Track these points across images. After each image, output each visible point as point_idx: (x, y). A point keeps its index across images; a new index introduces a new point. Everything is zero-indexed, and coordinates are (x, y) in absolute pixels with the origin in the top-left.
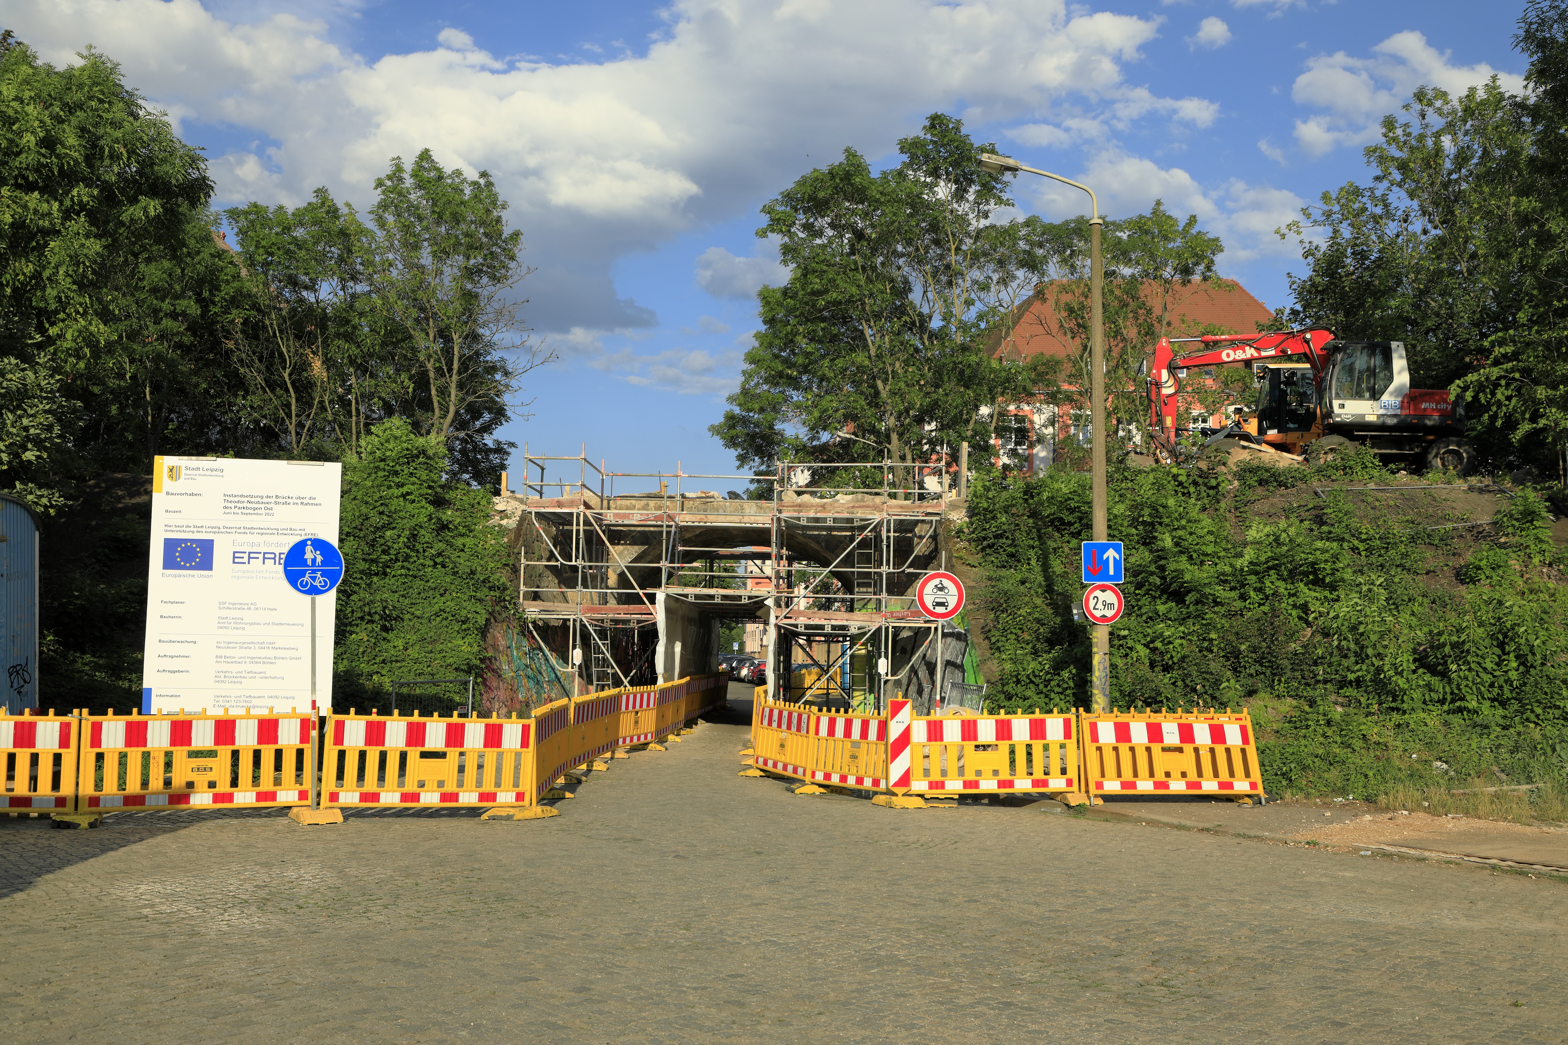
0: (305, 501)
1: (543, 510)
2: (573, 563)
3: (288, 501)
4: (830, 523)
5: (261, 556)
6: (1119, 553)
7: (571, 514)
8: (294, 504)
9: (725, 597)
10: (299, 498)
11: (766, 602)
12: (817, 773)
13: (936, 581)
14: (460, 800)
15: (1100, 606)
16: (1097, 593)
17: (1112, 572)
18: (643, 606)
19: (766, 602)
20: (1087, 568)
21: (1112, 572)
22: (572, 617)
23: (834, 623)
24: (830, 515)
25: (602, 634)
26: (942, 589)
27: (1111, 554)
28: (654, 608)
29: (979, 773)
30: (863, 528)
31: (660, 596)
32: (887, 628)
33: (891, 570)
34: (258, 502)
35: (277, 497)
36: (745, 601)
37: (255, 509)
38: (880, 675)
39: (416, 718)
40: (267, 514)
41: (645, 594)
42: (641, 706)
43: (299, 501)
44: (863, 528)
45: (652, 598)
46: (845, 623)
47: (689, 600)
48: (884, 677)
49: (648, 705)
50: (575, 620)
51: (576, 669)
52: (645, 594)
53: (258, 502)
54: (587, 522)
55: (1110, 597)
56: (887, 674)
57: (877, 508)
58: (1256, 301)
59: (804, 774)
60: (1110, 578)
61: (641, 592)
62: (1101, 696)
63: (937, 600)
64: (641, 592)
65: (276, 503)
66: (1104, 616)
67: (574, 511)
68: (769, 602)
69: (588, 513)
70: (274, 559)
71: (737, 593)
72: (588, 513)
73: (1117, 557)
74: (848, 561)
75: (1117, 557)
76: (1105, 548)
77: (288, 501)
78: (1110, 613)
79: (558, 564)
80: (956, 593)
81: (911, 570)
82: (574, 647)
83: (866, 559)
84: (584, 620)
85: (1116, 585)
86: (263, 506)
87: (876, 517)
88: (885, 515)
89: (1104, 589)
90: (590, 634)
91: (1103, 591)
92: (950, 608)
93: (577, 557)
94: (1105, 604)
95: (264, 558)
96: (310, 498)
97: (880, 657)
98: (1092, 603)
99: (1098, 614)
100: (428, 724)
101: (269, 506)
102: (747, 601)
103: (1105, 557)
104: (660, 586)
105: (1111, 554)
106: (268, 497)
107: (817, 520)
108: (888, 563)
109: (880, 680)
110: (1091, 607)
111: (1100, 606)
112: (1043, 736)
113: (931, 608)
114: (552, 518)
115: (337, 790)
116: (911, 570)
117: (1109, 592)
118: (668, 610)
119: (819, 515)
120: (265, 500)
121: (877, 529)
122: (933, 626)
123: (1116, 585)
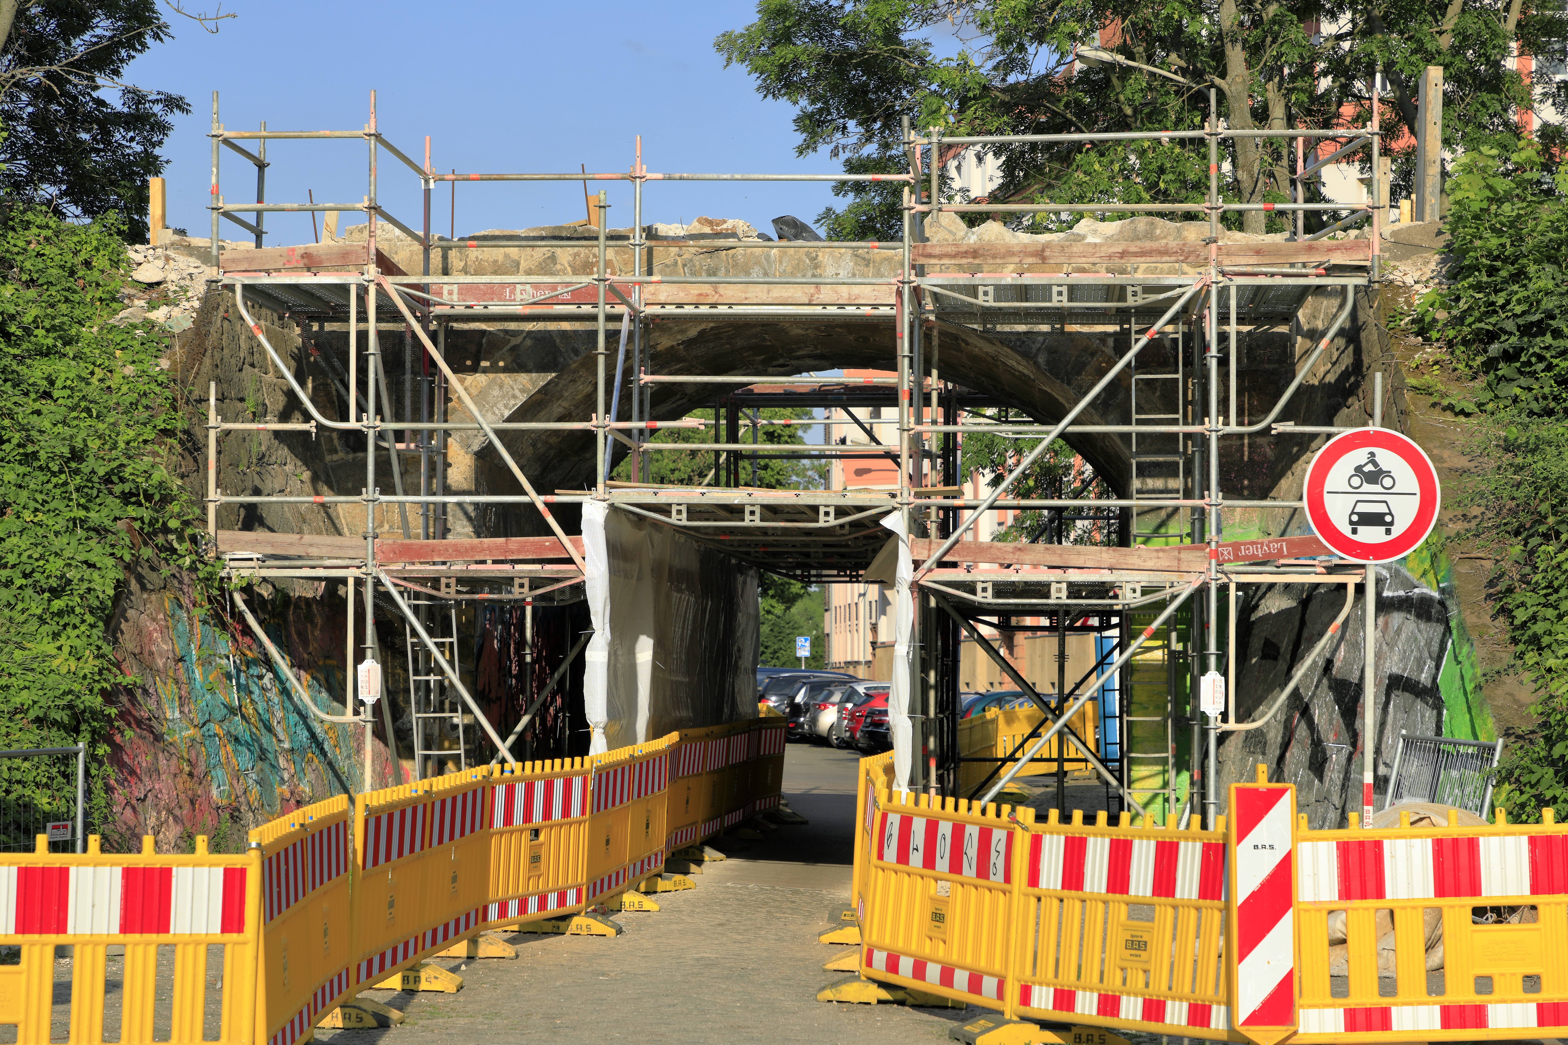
2: (352, 424)
4: (1059, 301)
7: (343, 289)
13: (1359, 456)
18: (547, 541)
22: (351, 574)
23: (1075, 576)
26: (1375, 476)
28: (578, 546)
29: (1484, 984)
32: (1223, 590)
33: (1233, 428)
47: (674, 519)
50: (359, 583)
63: (1362, 508)
67: (352, 279)
69: (390, 283)
71: (806, 498)
79: (311, 427)
80: (1415, 487)
82: (360, 657)
88: (1213, 275)
92: (1398, 530)
93: (361, 409)
102: (832, 521)
107: (1023, 292)
108: (1224, 409)
113: (1345, 529)
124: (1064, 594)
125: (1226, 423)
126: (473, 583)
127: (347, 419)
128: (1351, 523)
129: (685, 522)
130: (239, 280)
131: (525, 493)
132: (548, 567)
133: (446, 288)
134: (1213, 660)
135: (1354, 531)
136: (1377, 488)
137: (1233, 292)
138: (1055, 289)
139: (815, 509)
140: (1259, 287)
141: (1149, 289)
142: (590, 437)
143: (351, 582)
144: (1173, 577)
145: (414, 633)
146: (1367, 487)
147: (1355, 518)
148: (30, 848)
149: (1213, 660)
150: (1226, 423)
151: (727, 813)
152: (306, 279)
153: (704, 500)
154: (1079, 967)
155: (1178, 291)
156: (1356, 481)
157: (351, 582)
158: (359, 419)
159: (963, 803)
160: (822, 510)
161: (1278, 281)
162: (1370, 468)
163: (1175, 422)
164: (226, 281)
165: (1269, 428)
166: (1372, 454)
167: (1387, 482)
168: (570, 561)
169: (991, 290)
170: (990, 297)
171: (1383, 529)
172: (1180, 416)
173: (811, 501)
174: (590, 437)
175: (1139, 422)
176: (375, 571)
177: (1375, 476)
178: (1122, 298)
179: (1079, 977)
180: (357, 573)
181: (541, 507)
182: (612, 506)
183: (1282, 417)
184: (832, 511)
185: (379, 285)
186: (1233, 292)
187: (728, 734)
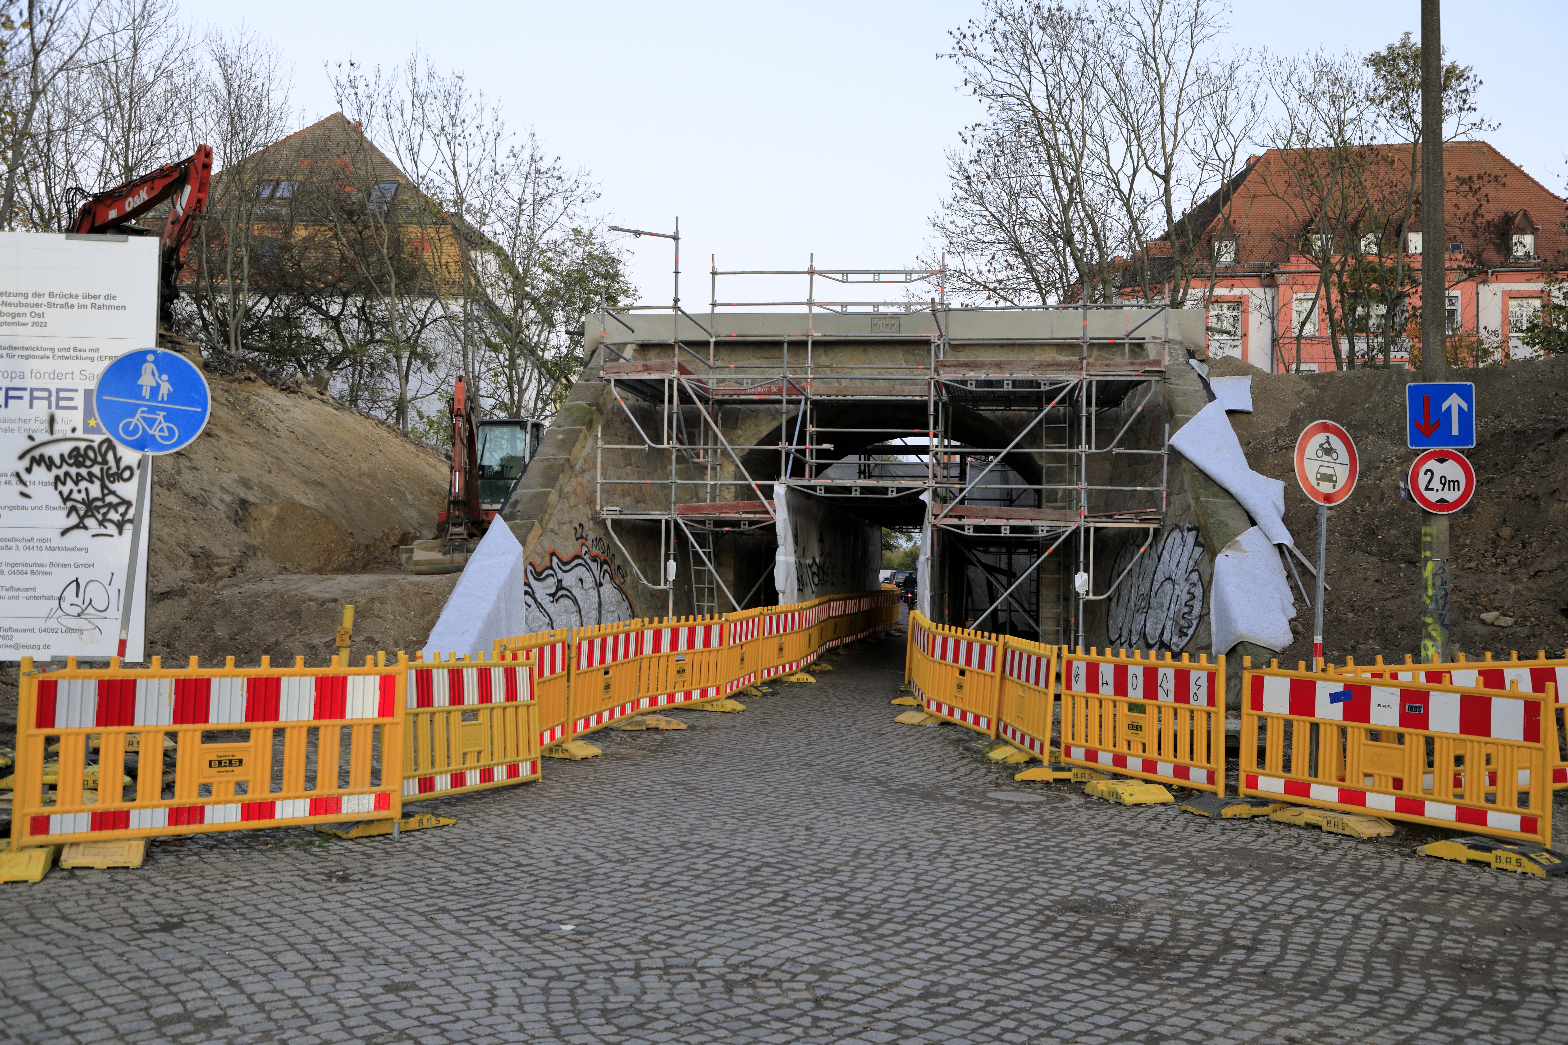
0: (99, 302)
1: (624, 377)
2: (665, 446)
3: (71, 301)
4: (1008, 388)
5: (26, 395)
6: (1468, 400)
7: (663, 381)
8: (81, 306)
10: (88, 296)
11: (922, 497)
14: (344, 810)
15: (1436, 484)
16: (1432, 464)
17: (1455, 431)
18: (757, 503)
19: (922, 497)
20: (1415, 424)
21: (1455, 431)
24: (1007, 376)
25: (701, 539)
26: (1329, 451)
27: (1454, 402)
28: (772, 505)
31: (779, 489)
32: (1087, 530)
33: (1093, 450)
34: (20, 304)
35: (51, 295)
37: (14, 315)
38: (1078, 594)
39: (265, 669)
40: (35, 324)
42: (615, 658)
43: (88, 302)
45: (768, 492)
47: (818, 493)
48: (1083, 597)
49: (626, 655)
53: (20, 304)
55: (1452, 470)
56: (1087, 593)
58: (1512, 164)
60: (1454, 441)
61: (753, 484)
62: (1438, 626)
64: (753, 484)
65: (50, 305)
66: (1442, 500)
67: (666, 376)
68: (925, 497)
69: (683, 379)
70: (48, 398)
71: (882, 483)
72: (683, 379)
73: (1465, 406)
74: (1033, 439)
75: (1465, 406)
76: (1446, 392)
77: (71, 301)
78: (1452, 496)
79: (646, 447)
82: (667, 559)
83: (1058, 437)
84: (680, 521)
85: (1462, 452)
86: (28, 310)
87: (1072, 379)
88: (1084, 375)
89: (1442, 459)
91: (1442, 461)
93: (670, 438)
94: (1444, 481)
95: (32, 399)
96: (108, 297)
97: (1077, 571)
98: (1423, 480)
99: (1432, 497)
100: (284, 682)
101: (38, 310)
102: (895, 495)
103: (1445, 406)
104: (779, 475)
105: (1454, 402)
106: (36, 295)
107: (989, 383)
108: (1089, 442)
109: (1077, 601)
110: (1422, 487)
111: (1436, 484)
112: (1422, 722)
113: (1314, 482)
114: (639, 387)
115: (46, 810)
117: (1451, 463)
118: (794, 510)
120: (31, 300)
121: (1071, 399)
122: (1152, 527)
123: (1462, 452)
126: (719, 523)
130: (613, 377)
136: (1329, 458)
141: (1052, 383)
142: (778, 452)
146: (1325, 458)
148: (1296, 668)
152: (645, 376)
154: (1192, 732)
156: (1320, 453)
159: (986, 634)
168: (767, 512)
174: (778, 452)
177: (1329, 451)
178: (1039, 386)
183: (1118, 446)
187: (860, 598)
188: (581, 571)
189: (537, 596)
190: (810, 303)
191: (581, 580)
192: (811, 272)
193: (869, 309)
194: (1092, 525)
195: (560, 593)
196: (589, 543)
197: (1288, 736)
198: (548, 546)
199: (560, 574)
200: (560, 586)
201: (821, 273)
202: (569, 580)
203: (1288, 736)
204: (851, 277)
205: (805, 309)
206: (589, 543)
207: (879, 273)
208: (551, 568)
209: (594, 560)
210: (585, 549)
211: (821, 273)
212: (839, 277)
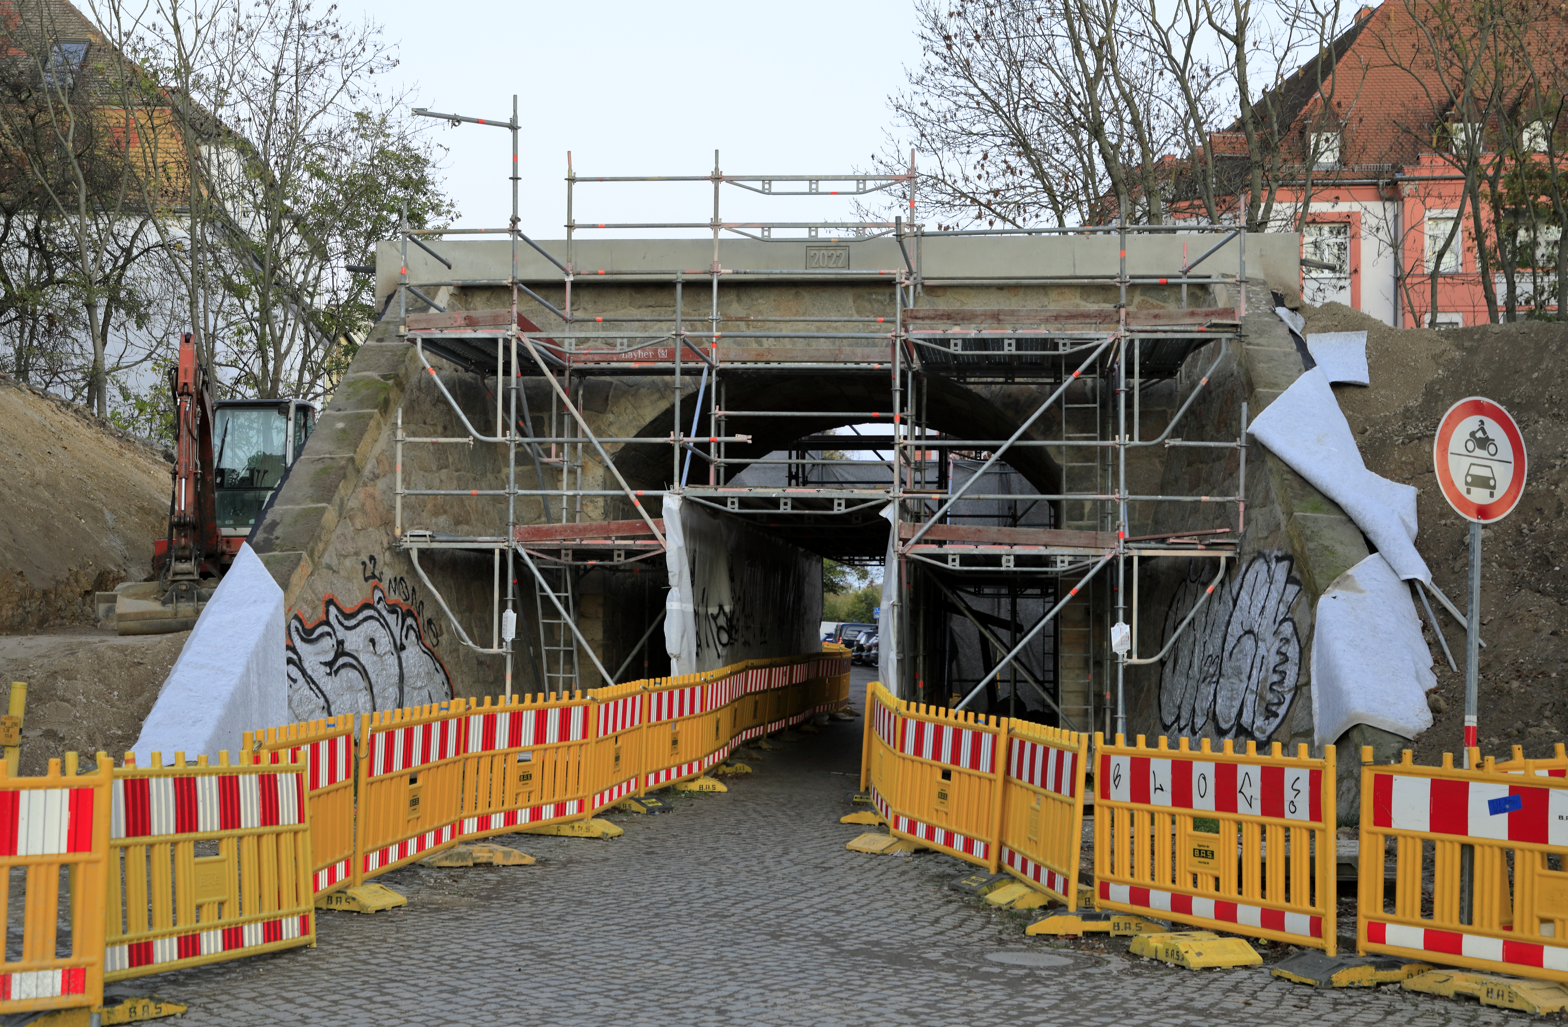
1: (437, 335)
2: (499, 438)
4: (1009, 350)
7: (495, 341)
9: (798, 502)
11: (883, 513)
12: (1113, 888)
18: (637, 523)
19: (883, 513)
22: (497, 547)
23: (1019, 550)
25: (554, 578)
28: (661, 526)
30: (1073, 362)
31: (671, 502)
32: (1129, 561)
33: (1137, 442)
36: (839, 510)
38: (1116, 656)
41: (637, 496)
44: (1073, 362)
45: (655, 507)
46: (1041, 551)
48: (1123, 661)
50: (503, 553)
51: (507, 649)
52: (637, 496)
54: (528, 366)
56: (1130, 654)
57: (1103, 318)
59: (1066, 892)
61: (632, 494)
67: (499, 334)
68: (889, 513)
69: (526, 338)
71: (824, 493)
72: (526, 338)
81: (1178, 442)
82: (503, 608)
84: (522, 552)
87: (1105, 336)
88: (1122, 331)
90: (533, 575)
93: (506, 427)
102: (843, 510)
107: (982, 343)
108: (1129, 430)
113: (1462, 488)
116: (1178, 442)
119: (987, 334)
122: (1223, 555)
124: (1012, 564)
125: (1131, 439)
126: (581, 554)
127: (495, 435)
128: (1467, 483)
129: (737, 510)
130: (419, 336)
131: (622, 489)
132: (638, 542)
133: (567, 342)
134: (1121, 613)
135: (1469, 492)
137: (1137, 344)
138: (1006, 342)
139: (831, 501)
140: (1157, 341)
141: (1075, 342)
142: (669, 448)
143: (497, 552)
144: (1092, 552)
145: (542, 589)
146: (1479, 452)
147: (1469, 479)
149: (1121, 613)
150: (1131, 439)
151: (770, 722)
152: (468, 334)
153: (751, 495)
155: (1096, 343)
156: (1471, 445)
157: (497, 552)
158: (504, 435)
160: (836, 502)
161: (1170, 336)
162: (1480, 435)
163: (1094, 439)
164: (410, 336)
165: (1162, 444)
166: (1482, 422)
167: (1492, 449)
168: (653, 537)
169: (960, 343)
170: (959, 347)
171: (1488, 491)
172: (1098, 435)
173: (828, 496)
174: (669, 448)
175: (1069, 439)
176: (514, 544)
178: (1055, 347)
179: (1152, 875)
180: (502, 546)
181: (633, 498)
182: (684, 498)
183: (1175, 434)
184: (843, 503)
185: (519, 339)
186: (1137, 344)
188: (372, 628)
189: (306, 665)
190: (715, 225)
191: (373, 641)
192: (717, 178)
193: (803, 233)
194: (1135, 553)
195: (341, 661)
196: (385, 585)
197: (1429, 864)
198: (323, 589)
199: (341, 633)
200: (340, 651)
201: (731, 180)
202: (354, 640)
203: (1429, 864)
204: (776, 186)
205: (707, 234)
206: (385, 585)
207: (818, 179)
208: (327, 623)
209: (393, 610)
210: (378, 594)
211: (731, 180)
212: (758, 185)
